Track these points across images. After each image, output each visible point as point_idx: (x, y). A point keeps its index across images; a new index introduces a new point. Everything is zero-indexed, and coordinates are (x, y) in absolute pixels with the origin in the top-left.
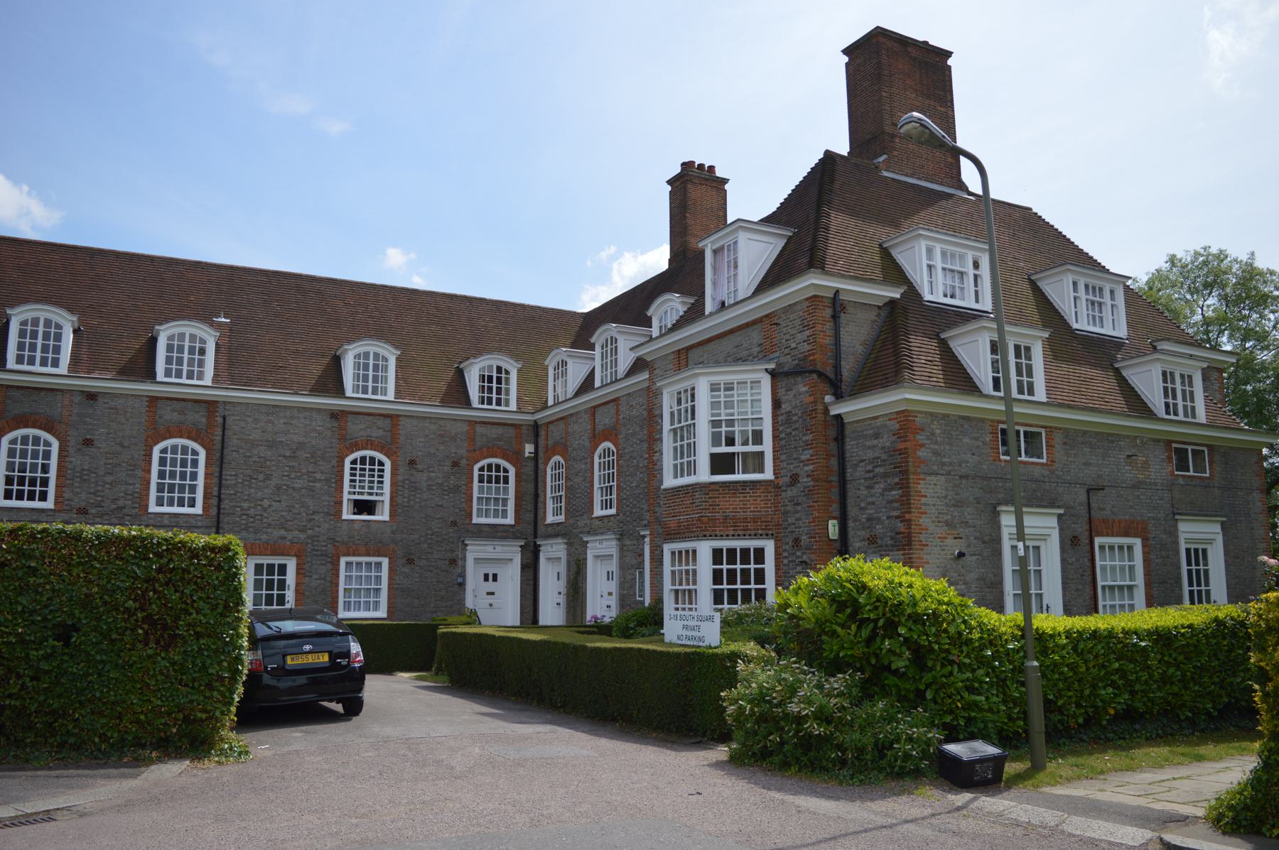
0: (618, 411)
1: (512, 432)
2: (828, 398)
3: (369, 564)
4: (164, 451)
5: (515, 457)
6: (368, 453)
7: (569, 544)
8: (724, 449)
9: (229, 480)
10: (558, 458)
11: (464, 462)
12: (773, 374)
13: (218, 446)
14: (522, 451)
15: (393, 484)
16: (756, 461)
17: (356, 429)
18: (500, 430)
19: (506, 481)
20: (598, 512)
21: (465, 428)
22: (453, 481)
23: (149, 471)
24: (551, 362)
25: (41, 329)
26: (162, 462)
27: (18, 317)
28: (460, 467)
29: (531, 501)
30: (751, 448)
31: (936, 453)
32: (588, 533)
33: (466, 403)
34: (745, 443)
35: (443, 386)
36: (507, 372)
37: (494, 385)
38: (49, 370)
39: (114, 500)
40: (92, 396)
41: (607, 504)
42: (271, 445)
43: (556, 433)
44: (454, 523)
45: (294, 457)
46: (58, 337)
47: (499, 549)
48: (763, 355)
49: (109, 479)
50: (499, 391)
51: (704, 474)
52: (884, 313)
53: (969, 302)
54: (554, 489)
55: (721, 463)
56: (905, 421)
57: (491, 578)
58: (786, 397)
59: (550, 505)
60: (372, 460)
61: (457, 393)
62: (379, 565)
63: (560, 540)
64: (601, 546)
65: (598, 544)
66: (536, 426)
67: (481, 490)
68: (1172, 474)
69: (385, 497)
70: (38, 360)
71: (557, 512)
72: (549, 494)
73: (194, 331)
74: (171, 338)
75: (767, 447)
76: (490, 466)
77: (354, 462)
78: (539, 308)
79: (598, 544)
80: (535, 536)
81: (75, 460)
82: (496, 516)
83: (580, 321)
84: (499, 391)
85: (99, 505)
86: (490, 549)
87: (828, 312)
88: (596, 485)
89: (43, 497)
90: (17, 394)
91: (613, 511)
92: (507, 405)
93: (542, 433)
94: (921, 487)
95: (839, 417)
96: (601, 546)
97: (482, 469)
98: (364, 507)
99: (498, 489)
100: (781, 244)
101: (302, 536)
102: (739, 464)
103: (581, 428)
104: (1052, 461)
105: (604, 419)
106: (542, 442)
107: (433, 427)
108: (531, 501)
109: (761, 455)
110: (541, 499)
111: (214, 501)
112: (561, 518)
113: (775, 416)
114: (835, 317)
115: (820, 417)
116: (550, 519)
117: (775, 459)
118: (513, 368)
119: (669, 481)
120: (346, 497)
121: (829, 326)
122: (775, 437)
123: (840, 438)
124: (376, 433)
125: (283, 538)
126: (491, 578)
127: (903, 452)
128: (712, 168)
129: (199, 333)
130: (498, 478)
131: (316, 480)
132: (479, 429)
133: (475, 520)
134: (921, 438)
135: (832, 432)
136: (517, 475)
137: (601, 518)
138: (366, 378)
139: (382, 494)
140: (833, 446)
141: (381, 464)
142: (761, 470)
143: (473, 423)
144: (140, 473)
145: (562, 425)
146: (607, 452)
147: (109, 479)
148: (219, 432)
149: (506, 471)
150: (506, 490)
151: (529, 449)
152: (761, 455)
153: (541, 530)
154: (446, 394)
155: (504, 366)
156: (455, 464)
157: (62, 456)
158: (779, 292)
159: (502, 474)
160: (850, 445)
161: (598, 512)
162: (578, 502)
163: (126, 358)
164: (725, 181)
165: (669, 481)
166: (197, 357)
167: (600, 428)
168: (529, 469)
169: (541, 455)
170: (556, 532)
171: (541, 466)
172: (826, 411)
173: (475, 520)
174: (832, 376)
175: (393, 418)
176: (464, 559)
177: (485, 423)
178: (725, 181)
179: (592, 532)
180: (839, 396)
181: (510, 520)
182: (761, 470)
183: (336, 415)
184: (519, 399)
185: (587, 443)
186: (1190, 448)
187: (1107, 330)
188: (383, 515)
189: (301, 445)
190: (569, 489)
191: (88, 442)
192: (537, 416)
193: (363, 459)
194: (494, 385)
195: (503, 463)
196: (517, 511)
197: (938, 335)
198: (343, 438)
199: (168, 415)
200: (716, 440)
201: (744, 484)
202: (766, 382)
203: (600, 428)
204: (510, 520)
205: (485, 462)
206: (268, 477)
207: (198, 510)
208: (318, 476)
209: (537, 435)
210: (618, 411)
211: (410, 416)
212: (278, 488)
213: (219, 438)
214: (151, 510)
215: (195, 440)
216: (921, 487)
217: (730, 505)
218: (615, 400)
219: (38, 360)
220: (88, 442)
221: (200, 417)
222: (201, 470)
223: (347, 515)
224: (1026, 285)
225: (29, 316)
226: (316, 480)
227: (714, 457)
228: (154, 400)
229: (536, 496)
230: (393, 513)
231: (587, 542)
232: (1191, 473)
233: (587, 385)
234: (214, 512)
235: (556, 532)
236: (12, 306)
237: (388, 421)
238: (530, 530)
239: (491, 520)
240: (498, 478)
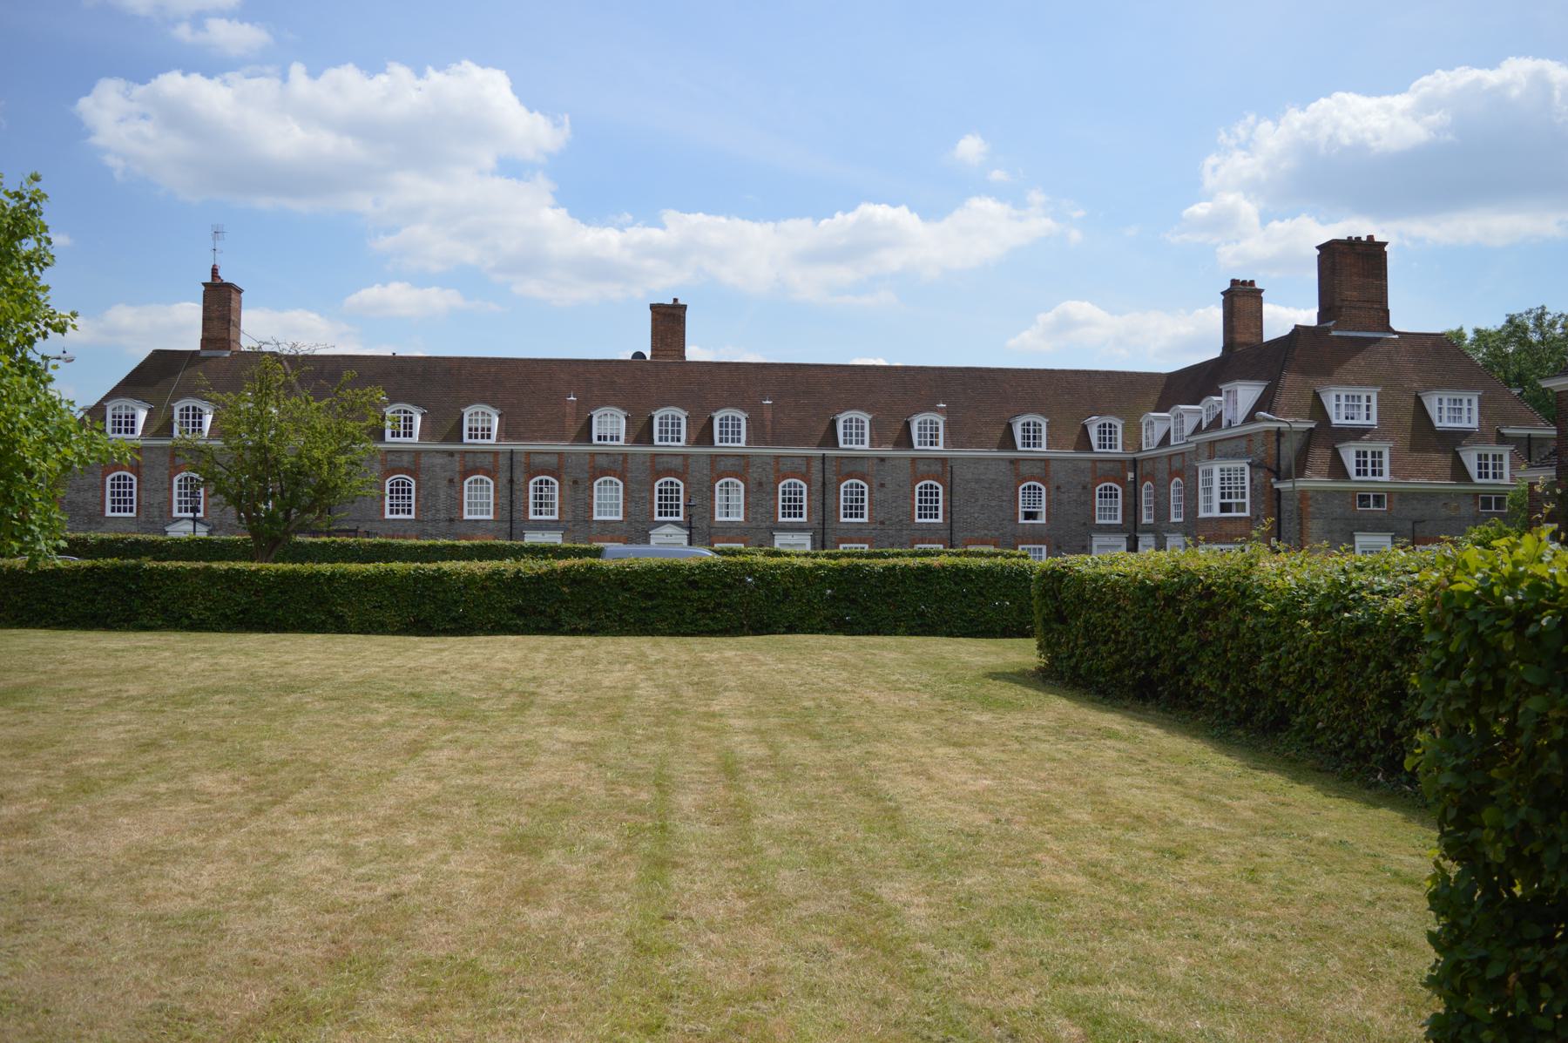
0: (1184, 461)
1: (1119, 465)
2: (1273, 480)
3: (1035, 549)
5: (1122, 481)
6: (929, 482)
7: (1157, 538)
8: (1226, 500)
9: (956, 503)
10: (1148, 483)
11: (1089, 486)
12: (1249, 464)
13: (949, 484)
14: (1126, 477)
15: (1048, 501)
16: (1241, 507)
17: (1024, 469)
18: (1111, 465)
19: (1116, 496)
20: (1173, 519)
21: (1090, 464)
22: (1083, 498)
23: (914, 500)
24: (1144, 421)
28: (1088, 490)
29: (1132, 509)
30: (1240, 500)
31: (1318, 509)
32: (1168, 532)
33: (1090, 448)
34: (1237, 497)
35: (1075, 437)
36: (1115, 427)
37: (1107, 436)
39: (898, 516)
40: (882, 460)
41: (1177, 515)
42: (978, 481)
43: (1148, 467)
44: (1085, 524)
45: (990, 488)
47: (1112, 539)
48: (1246, 454)
49: (894, 505)
50: (1110, 439)
51: (1216, 513)
52: (1306, 434)
53: (1361, 421)
54: (1147, 502)
55: (1225, 508)
56: (1304, 494)
58: (1255, 477)
59: (1144, 512)
60: (1035, 487)
61: (1084, 443)
62: (1040, 550)
63: (1150, 535)
66: (1135, 461)
67: (1101, 503)
68: (1478, 511)
69: (1042, 509)
71: (1149, 516)
72: (1144, 505)
73: (674, 413)
74: (661, 418)
75: (1247, 500)
76: (1106, 488)
77: (1024, 489)
78: (1136, 373)
80: (1135, 530)
81: (877, 495)
82: (1110, 519)
83: (1164, 380)
84: (1110, 439)
85: (890, 519)
86: (1107, 539)
87: (1274, 438)
88: (1172, 503)
89: (862, 516)
90: (845, 461)
91: (1181, 520)
92: (1116, 448)
93: (1139, 466)
94: (1310, 525)
95: (1278, 489)
97: (1101, 490)
98: (1029, 516)
99: (1111, 502)
100: (1262, 389)
101: (997, 534)
102: (1234, 507)
103: (1163, 467)
104: (1390, 509)
105: (1177, 464)
106: (1138, 472)
107: (1070, 465)
108: (1132, 509)
109: (1244, 504)
110: (1139, 508)
111: (949, 515)
112: (1151, 521)
113: (1251, 486)
114: (1278, 441)
115: (1268, 488)
116: (1145, 520)
117: (1251, 507)
118: (1119, 424)
119: (1202, 514)
120: (1020, 510)
121: (1275, 444)
122: (1251, 496)
123: (1279, 499)
124: (1036, 471)
125: (986, 535)
127: (1301, 509)
128: (1252, 283)
130: (1111, 495)
131: (1003, 501)
132: (1098, 465)
133: (1098, 522)
134: (1310, 502)
135: (1275, 496)
136: (1123, 492)
137: (1175, 523)
138: (1029, 438)
140: (1275, 503)
141: (1040, 489)
142: (1244, 511)
143: (1094, 461)
144: (909, 501)
145: (1151, 462)
146: (1177, 484)
147: (894, 505)
148: (949, 475)
150: (1116, 502)
151: (1130, 475)
152: (1244, 504)
153: (1139, 527)
154: (1077, 443)
155: (1113, 423)
156: (1084, 488)
157: (870, 494)
160: (1283, 502)
161: (1173, 519)
162: (1161, 512)
163: (896, 435)
164: (1261, 291)
165: (1202, 514)
167: (1174, 468)
168: (1131, 488)
169: (1138, 479)
170: (1148, 529)
171: (1139, 487)
172: (1272, 486)
173: (1098, 522)
174: (1275, 469)
175: (1046, 461)
176: (1091, 545)
177: (1102, 461)
178: (1261, 291)
179: (1169, 531)
180: (1279, 479)
181: (1119, 521)
182: (1244, 511)
183: (1013, 462)
184: (1123, 443)
185: (1166, 476)
186: (1493, 497)
187: (1464, 424)
188: (1042, 520)
189: (994, 481)
190: (1156, 503)
191: (882, 485)
192: (1136, 456)
193: (1029, 487)
194: (1107, 436)
196: (1123, 515)
197: (1334, 445)
198: (1017, 475)
199: (922, 467)
200: (1223, 496)
201: (1236, 518)
202: (1247, 469)
203: (1174, 468)
204: (1119, 521)
205: (1103, 485)
206: (977, 500)
207: (940, 520)
208: (1004, 498)
209: (1135, 466)
210: (1184, 461)
211: (1056, 459)
212: (982, 506)
213: (949, 479)
215: (937, 481)
216: (1310, 525)
217: (1229, 528)
218: (1183, 454)
220: (882, 485)
221: (939, 468)
222: (941, 498)
223: (1021, 521)
224: (1410, 403)
226: (1003, 501)
227: (1222, 505)
228: (914, 460)
229: (1136, 505)
230: (1047, 519)
232: (1493, 510)
233: (1165, 440)
234: (949, 521)
235: (1148, 529)
237: (1043, 464)
238: (1132, 527)
239: (1107, 522)
240: (1111, 495)
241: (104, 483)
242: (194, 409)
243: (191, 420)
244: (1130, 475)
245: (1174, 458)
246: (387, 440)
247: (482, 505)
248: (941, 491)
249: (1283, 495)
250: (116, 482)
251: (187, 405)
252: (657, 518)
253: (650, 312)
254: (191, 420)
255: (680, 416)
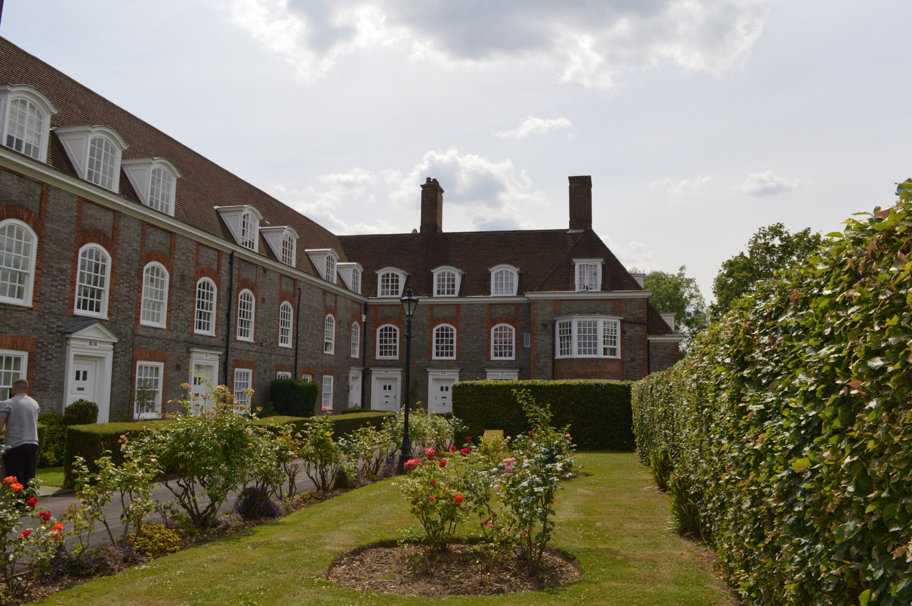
4: (496, 330)
6: (388, 325)
14: (361, 319)
25: (390, 278)
26: (438, 335)
27: (436, 272)
30: (613, 347)
38: (451, 295)
46: (453, 280)
47: (505, 374)
57: (444, 389)
64: (90, 347)
65: (205, 355)
70: (446, 292)
73: (449, 271)
74: (439, 275)
76: (386, 329)
79: (205, 355)
89: (452, 355)
96: (90, 347)
97: (382, 330)
126: (444, 389)
129: (452, 272)
139: (331, 339)
149: (395, 330)
158: (119, 200)
159: (393, 332)
166: (395, 284)
195: (393, 326)
205: (383, 326)
214: (492, 359)
219: (446, 292)
225: (441, 271)
231: (428, 372)
236: (434, 268)
241: (431, 333)
242: (393, 275)
243: (390, 284)
244: (364, 318)
245: (329, 295)
246: (434, 296)
247: (390, 347)
248: (455, 332)
249: (650, 345)
250: (498, 332)
251: (387, 272)
252: (78, 312)
253: (568, 184)
254: (390, 284)
255: (454, 273)
